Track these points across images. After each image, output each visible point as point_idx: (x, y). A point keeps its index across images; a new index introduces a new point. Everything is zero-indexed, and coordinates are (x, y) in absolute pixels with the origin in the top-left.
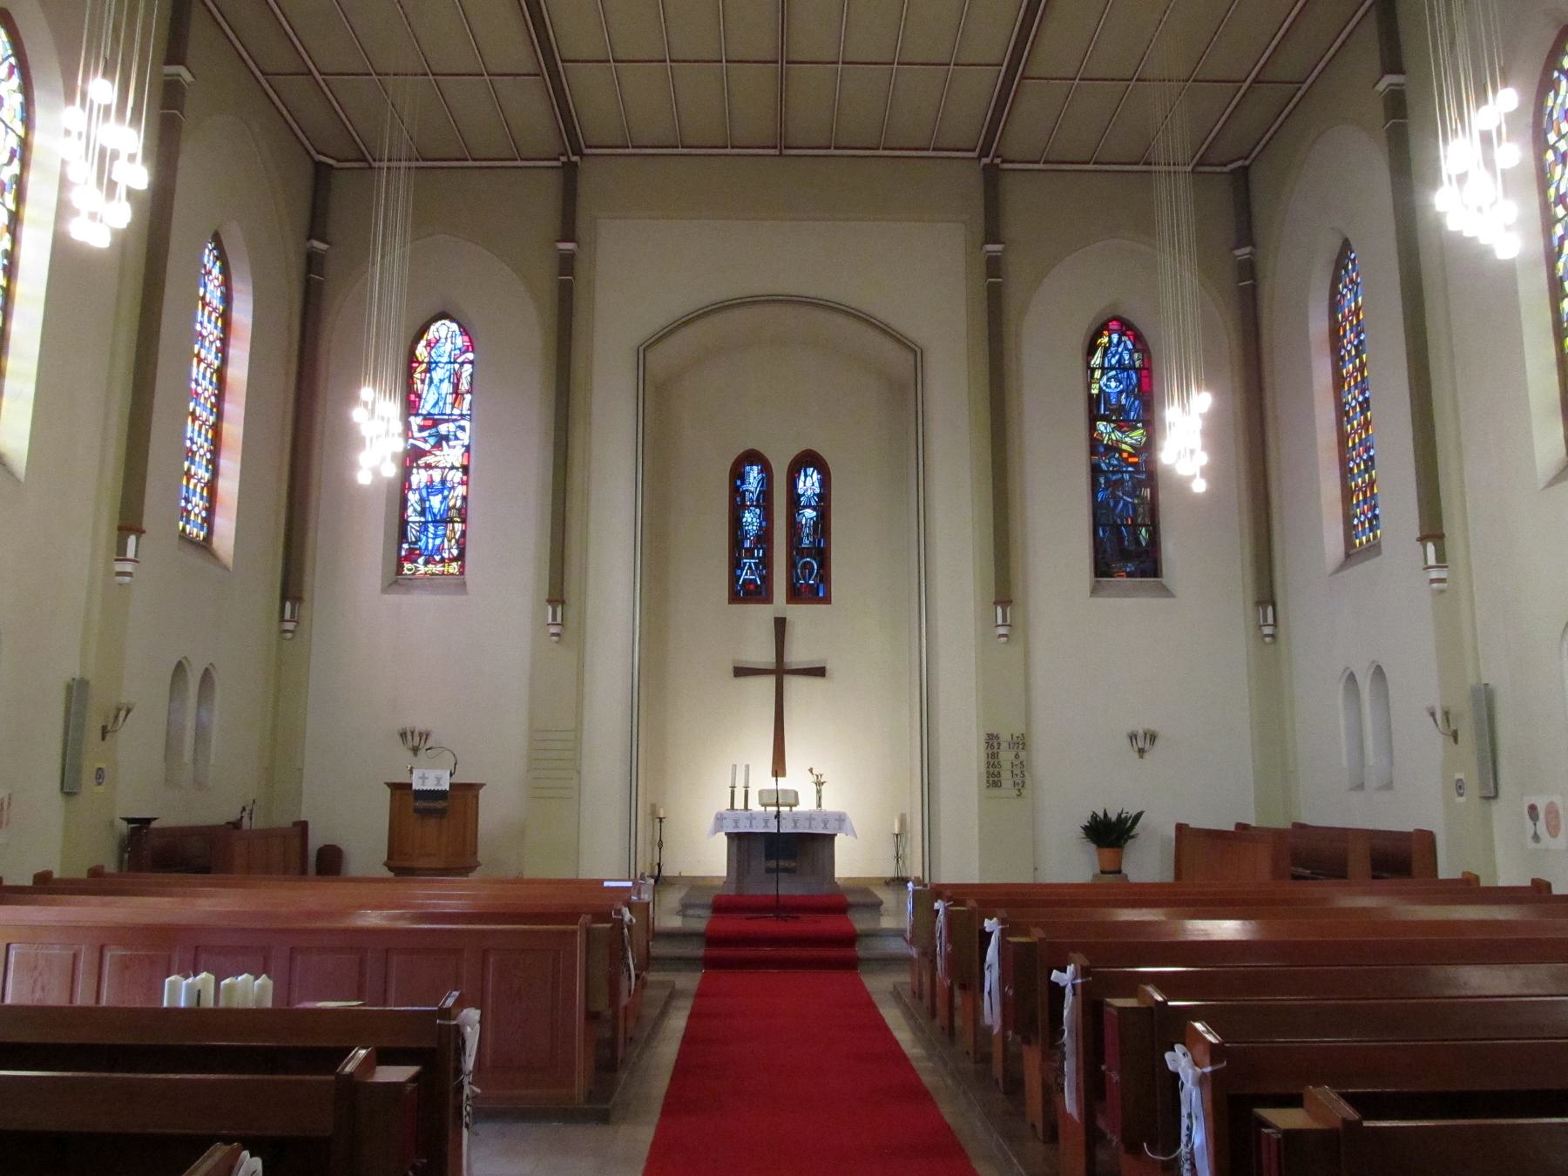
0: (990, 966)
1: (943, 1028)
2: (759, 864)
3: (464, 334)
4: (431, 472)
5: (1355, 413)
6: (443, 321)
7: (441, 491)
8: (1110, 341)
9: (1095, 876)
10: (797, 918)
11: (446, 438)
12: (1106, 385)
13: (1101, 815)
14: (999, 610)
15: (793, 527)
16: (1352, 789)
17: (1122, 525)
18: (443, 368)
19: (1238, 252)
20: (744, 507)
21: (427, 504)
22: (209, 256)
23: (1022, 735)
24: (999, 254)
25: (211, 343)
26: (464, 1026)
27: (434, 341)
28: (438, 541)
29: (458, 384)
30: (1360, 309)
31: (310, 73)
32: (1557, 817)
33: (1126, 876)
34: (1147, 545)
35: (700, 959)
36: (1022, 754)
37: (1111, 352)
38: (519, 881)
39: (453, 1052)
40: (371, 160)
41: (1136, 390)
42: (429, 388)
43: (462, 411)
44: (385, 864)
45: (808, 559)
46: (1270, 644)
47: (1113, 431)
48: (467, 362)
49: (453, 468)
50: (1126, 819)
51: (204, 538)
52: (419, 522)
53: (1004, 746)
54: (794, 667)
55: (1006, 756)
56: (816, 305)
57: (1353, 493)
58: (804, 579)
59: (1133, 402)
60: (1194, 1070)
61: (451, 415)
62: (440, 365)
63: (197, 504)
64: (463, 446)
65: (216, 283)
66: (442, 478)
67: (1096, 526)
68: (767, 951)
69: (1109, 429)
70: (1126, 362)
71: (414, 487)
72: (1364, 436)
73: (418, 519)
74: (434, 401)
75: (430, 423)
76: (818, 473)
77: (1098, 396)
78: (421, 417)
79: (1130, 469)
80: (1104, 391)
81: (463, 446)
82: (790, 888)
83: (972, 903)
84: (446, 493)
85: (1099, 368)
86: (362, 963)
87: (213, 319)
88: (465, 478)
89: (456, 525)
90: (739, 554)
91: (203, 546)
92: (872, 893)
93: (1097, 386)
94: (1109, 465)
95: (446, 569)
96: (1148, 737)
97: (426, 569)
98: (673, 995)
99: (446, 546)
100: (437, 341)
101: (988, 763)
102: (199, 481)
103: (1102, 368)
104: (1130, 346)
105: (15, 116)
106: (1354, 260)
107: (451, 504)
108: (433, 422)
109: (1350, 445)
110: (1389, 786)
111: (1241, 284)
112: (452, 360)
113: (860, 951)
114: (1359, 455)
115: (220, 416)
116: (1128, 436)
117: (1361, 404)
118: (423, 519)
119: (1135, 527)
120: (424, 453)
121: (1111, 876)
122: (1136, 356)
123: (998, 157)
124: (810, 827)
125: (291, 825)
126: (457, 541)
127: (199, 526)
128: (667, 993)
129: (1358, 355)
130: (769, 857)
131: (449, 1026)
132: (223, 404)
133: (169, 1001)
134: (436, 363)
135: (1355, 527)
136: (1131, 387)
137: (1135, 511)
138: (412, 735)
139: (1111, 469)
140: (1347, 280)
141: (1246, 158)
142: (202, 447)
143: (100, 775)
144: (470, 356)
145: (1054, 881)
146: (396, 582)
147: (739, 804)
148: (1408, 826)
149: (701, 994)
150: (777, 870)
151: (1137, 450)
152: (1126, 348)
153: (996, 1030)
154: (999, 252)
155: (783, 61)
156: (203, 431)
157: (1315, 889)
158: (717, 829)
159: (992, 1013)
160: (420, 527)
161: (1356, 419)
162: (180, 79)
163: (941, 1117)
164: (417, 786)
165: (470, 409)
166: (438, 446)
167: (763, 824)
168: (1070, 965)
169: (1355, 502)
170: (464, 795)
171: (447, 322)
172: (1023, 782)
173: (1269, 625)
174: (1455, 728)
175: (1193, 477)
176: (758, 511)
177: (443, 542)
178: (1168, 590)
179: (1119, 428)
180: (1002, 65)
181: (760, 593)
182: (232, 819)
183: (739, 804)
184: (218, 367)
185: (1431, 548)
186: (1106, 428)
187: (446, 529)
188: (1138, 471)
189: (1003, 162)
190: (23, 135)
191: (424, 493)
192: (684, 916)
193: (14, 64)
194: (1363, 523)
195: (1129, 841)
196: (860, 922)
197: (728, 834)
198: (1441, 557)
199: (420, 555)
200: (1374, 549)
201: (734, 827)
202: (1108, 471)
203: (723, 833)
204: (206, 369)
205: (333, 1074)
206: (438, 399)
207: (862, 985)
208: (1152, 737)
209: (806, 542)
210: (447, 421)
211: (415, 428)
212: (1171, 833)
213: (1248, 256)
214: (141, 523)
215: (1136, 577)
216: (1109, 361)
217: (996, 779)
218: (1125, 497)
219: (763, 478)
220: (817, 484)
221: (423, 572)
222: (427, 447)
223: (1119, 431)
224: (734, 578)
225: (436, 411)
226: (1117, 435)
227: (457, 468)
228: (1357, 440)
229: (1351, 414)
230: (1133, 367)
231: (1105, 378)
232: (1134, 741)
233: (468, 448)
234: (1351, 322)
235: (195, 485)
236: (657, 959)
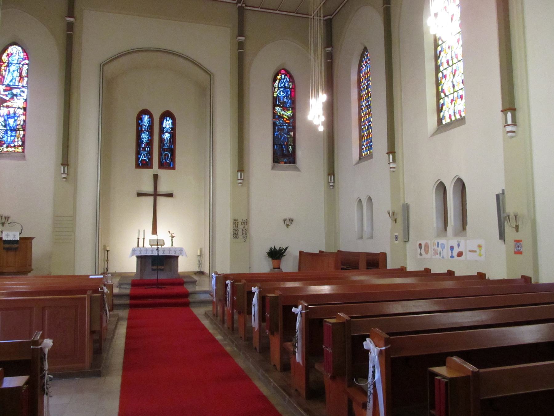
0: (254, 305)
1: (229, 328)
2: (149, 267)
3: (24, 52)
4: (9, 109)
6: (15, 46)
8: (281, 78)
9: (271, 270)
10: (165, 287)
12: (279, 94)
13: (273, 248)
14: (239, 174)
15: (161, 140)
17: (283, 145)
18: (15, 66)
19: (327, 49)
24: (243, 41)
26: (45, 348)
27: (10, 54)
28: (13, 138)
30: (368, 72)
32: (428, 247)
33: (282, 270)
34: (292, 152)
36: (246, 227)
37: (281, 82)
38: (49, 276)
39: (39, 360)
41: (290, 96)
43: (23, 84)
45: (167, 153)
46: (332, 189)
47: (281, 111)
48: (25, 64)
49: (19, 108)
50: (282, 250)
52: (4, 130)
53: (240, 223)
54: (161, 193)
55: (240, 227)
56: (173, 54)
57: (363, 137)
58: (165, 160)
59: (289, 100)
60: (377, 348)
62: (13, 64)
64: (24, 99)
66: (14, 112)
67: (274, 144)
68: (149, 301)
69: (280, 110)
70: (287, 86)
72: (367, 117)
73: (3, 128)
75: (8, 88)
76: (171, 120)
77: (276, 97)
78: (5, 86)
79: (287, 125)
80: (279, 96)
81: (24, 99)
82: (162, 276)
83: (244, 281)
84: (16, 118)
85: (277, 87)
90: (140, 149)
92: (192, 278)
93: (276, 93)
94: (279, 123)
95: (16, 150)
96: (290, 220)
97: (7, 149)
98: (119, 319)
100: (12, 54)
101: (234, 229)
103: (278, 87)
104: (288, 80)
106: (367, 55)
107: (18, 123)
108: (9, 88)
109: (363, 120)
110: (371, 237)
111: (327, 61)
112: (19, 63)
113: (190, 299)
114: (365, 124)
116: (286, 113)
117: (367, 106)
118: (5, 129)
119: (288, 146)
120: (6, 101)
121: (277, 269)
122: (290, 83)
124: (169, 253)
126: (21, 139)
128: (117, 319)
129: (367, 89)
130: (153, 265)
131: (38, 349)
134: (11, 63)
135: (363, 149)
136: (288, 95)
137: (288, 140)
139: (280, 124)
140: (365, 62)
141: (331, 15)
147: (141, 245)
148: (378, 251)
149: (129, 319)
150: (157, 270)
151: (289, 118)
152: (287, 81)
153: (256, 329)
154: (243, 40)
157: (347, 274)
158: (133, 254)
159: (255, 323)
160: (4, 132)
161: (365, 111)
163: (236, 364)
166: (12, 98)
167: (174, 253)
168: (300, 305)
169: (363, 140)
170: (26, 241)
171: (16, 47)
172: (246, 236)
173: (332, 182)
175: (319, 125)
176: (147, 133)
177: (15, 138)
178: (298, 169)
179: (283, 110)
181: (148, 165)
183: (141, 245)
185: (391, 156)
186: (279, 109)
187: (16, 133)
188: (289, 126)
189: (247, 6)
191: (6, 118)
192: (120, 288)
194: (366, 148)
195: (283, 257)
196: (190, 288)
197: (137, 256)
198: (394, 159)
199: (4, 144)
200: (370, 156)
201: (151, 253)
202: (279, 125)
203: (135, 256)
206: (12, 79)
207: (192, 312)
208: (291, 221)
209: (166, 146)
212: (297, 254)
213: (330, 51)
216: (281, 85)
218: (284, 135)
219: (150, 121)
220: (171, 124)
222: (7, 98)
223: (283, 111)
224: (137, 159)
225: (11, 84)
226: (282, 112)
227: (21, 108)
228: (365, 119)
229: (363, 109)
230: (289, 88)
232: (285, 222)
234: (365, 77)
236: (116, 305)
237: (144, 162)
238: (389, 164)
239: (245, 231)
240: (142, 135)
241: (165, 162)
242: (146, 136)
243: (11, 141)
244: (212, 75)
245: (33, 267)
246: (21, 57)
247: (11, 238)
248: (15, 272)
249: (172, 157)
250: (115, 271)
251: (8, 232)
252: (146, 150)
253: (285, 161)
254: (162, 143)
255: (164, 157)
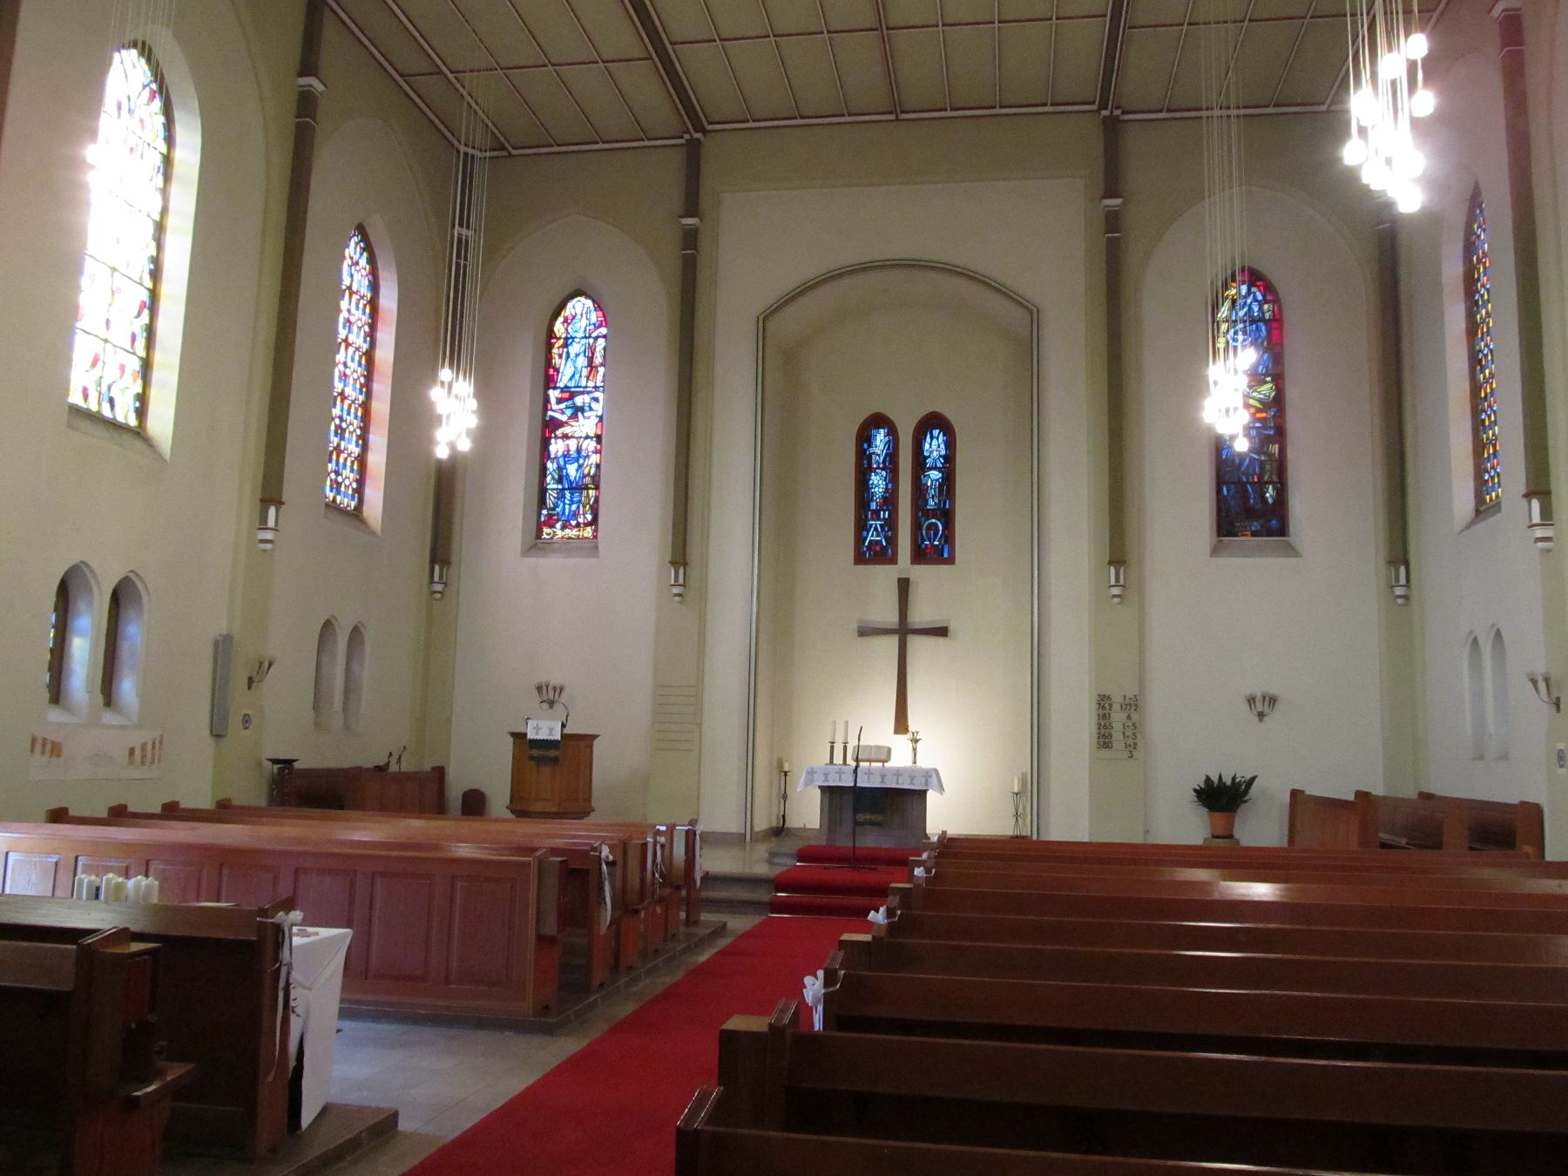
4: (567, 442)
5: (1487, 361)
6: (579, 298)
7: (577, 460)
8: (1239, 292)
9: (1205, 840)
10: (876, 869)
11: (582, 409)
13: (1215, 779)
14: (1112, 570)
15: (919, 490)
16: (1473, 759)
17: (1248, 482)
20: (870, 470)
21: (565, 471)
22: (355, 248)
23: (1135, 696)
25: (360, 328)
27: (570, 317)
28: (574, 507)
29: (592, 357)
31: (440, 72)
35: (767, 904)
36: (1135, 716)
40: (510, 149)
42: (566, 361)
44: (507, 808)
45: (933, 520)
46: (1404, 605)
49: (587, 437)
50: (1240, 784)
51: (355, 507)
52: (557, 489)
53: (1116, 707)
54: (916, 627)
55: (1118, 717)
58: (930, 540)
61: (586, 387)
63: (349, 477)
64: (597, 416)
65: (364, 272)
70: (1256, 314)
71: (552, 456)
73: (555, 486)
74: (571, 375)
75: (566, 395)
78: (559, 391)
81: (597, 416)
82: (871, 840)
84: (581, 461)
86: (352, 883)
87: (361, 306)
88: (598, 447)
89: (590, 491)
91: (354, 515)
97: (563, 533)
99: (581, 512)
100: (574, 317)
101: (1099, 724)
102: (349, 455)
104: (1260, 297)
105: (157, 136)
107: (586, 471)
115: (369, 395)
116: (1255, 391)
118: (560, 487)
119: (1261, 486)
120: (561, 424)
123: (1117, 108)
125: (429, 769)
126: (591, 507)
127: (350, 497)
131: (266, 923)
132: (372, 384)
133: (11, 888)
134: (572, 338)
138: (547, 687)
142: (351, 424)
143: (246, 720)
144: (604, 331)
145: (1166, 842)
146: (535, 546)
147: (838, 759)
148: (1513, 798)
152: (1255, 300)
155: (883, 28)
156: (353, 410)
160: (557, 493)
162: (312, 89)
164: (531, 736)
165: (603, 382)
166: (574, 416)
167: (880, 779)
171: (582, 299)
172: (1135, 744)
173: (1401, 586)
174: (1557, 695)
175: (1233, 438)
176: (884, 473)
177: (578, 507)
180: (1105, 16)
182: (381, 764)
183: (838, 759)
184: (367, 350)
185: (1536, 504)
189: (1124, 113)
190: (165, 151)
191: (562, 461)
193: (155, 89)
198: (1547, 513)
199: (558, 520)
204: (355, 352)
205: (74, 944)
208: (1272, 701)
209: (931, 504)
210: (583, 393)
211: (553, 401)
214: (281, 498)
215: (1262, 536)
217: (1107, 740)
219: (889, 441)
220: (942, 446)
221: (560, 536)
222: (564, 418)
224: (859, 540)
225: (572, 384)
227: (592, 438)
231: (1232, 331)
233: (601, 418)
235: (346, 460)
237: (878, 548)
238: (1530, 527)
239: (1132, 727)
240: (870, 479)
241: (929, 546)
242: (880, 482)
243: (572, 513)
244: (1035, 310)
245: (594, 804)
246: (591, 322)
247: (543, 735)
248: (557, 813)
249: (946, 532)
250: (805, 825)
251: (539, 722)
252: (882, 517)
253: (1253, 529)
254: (920, 496)
255: (927, 533)
